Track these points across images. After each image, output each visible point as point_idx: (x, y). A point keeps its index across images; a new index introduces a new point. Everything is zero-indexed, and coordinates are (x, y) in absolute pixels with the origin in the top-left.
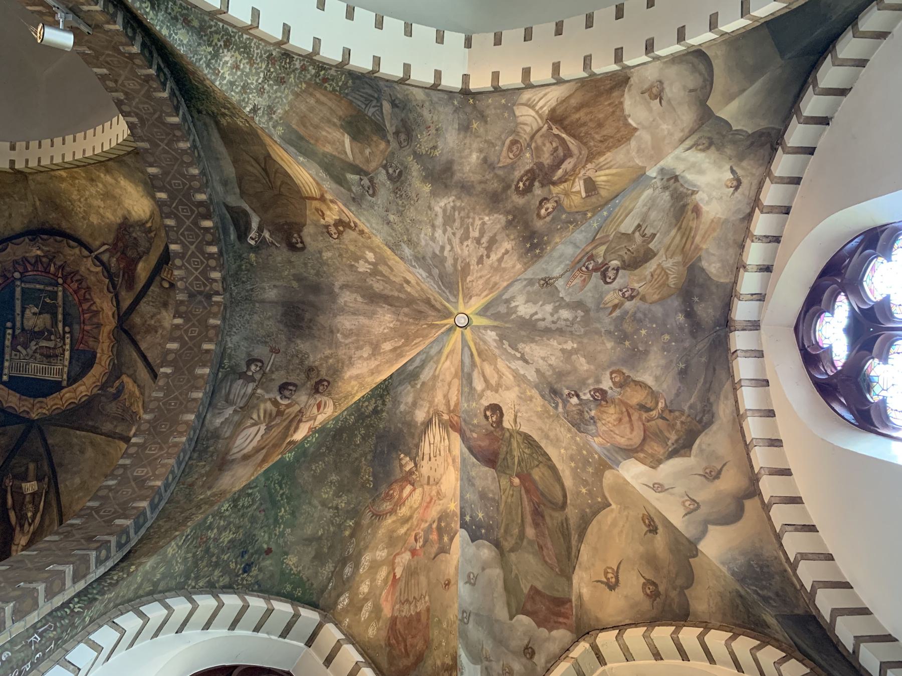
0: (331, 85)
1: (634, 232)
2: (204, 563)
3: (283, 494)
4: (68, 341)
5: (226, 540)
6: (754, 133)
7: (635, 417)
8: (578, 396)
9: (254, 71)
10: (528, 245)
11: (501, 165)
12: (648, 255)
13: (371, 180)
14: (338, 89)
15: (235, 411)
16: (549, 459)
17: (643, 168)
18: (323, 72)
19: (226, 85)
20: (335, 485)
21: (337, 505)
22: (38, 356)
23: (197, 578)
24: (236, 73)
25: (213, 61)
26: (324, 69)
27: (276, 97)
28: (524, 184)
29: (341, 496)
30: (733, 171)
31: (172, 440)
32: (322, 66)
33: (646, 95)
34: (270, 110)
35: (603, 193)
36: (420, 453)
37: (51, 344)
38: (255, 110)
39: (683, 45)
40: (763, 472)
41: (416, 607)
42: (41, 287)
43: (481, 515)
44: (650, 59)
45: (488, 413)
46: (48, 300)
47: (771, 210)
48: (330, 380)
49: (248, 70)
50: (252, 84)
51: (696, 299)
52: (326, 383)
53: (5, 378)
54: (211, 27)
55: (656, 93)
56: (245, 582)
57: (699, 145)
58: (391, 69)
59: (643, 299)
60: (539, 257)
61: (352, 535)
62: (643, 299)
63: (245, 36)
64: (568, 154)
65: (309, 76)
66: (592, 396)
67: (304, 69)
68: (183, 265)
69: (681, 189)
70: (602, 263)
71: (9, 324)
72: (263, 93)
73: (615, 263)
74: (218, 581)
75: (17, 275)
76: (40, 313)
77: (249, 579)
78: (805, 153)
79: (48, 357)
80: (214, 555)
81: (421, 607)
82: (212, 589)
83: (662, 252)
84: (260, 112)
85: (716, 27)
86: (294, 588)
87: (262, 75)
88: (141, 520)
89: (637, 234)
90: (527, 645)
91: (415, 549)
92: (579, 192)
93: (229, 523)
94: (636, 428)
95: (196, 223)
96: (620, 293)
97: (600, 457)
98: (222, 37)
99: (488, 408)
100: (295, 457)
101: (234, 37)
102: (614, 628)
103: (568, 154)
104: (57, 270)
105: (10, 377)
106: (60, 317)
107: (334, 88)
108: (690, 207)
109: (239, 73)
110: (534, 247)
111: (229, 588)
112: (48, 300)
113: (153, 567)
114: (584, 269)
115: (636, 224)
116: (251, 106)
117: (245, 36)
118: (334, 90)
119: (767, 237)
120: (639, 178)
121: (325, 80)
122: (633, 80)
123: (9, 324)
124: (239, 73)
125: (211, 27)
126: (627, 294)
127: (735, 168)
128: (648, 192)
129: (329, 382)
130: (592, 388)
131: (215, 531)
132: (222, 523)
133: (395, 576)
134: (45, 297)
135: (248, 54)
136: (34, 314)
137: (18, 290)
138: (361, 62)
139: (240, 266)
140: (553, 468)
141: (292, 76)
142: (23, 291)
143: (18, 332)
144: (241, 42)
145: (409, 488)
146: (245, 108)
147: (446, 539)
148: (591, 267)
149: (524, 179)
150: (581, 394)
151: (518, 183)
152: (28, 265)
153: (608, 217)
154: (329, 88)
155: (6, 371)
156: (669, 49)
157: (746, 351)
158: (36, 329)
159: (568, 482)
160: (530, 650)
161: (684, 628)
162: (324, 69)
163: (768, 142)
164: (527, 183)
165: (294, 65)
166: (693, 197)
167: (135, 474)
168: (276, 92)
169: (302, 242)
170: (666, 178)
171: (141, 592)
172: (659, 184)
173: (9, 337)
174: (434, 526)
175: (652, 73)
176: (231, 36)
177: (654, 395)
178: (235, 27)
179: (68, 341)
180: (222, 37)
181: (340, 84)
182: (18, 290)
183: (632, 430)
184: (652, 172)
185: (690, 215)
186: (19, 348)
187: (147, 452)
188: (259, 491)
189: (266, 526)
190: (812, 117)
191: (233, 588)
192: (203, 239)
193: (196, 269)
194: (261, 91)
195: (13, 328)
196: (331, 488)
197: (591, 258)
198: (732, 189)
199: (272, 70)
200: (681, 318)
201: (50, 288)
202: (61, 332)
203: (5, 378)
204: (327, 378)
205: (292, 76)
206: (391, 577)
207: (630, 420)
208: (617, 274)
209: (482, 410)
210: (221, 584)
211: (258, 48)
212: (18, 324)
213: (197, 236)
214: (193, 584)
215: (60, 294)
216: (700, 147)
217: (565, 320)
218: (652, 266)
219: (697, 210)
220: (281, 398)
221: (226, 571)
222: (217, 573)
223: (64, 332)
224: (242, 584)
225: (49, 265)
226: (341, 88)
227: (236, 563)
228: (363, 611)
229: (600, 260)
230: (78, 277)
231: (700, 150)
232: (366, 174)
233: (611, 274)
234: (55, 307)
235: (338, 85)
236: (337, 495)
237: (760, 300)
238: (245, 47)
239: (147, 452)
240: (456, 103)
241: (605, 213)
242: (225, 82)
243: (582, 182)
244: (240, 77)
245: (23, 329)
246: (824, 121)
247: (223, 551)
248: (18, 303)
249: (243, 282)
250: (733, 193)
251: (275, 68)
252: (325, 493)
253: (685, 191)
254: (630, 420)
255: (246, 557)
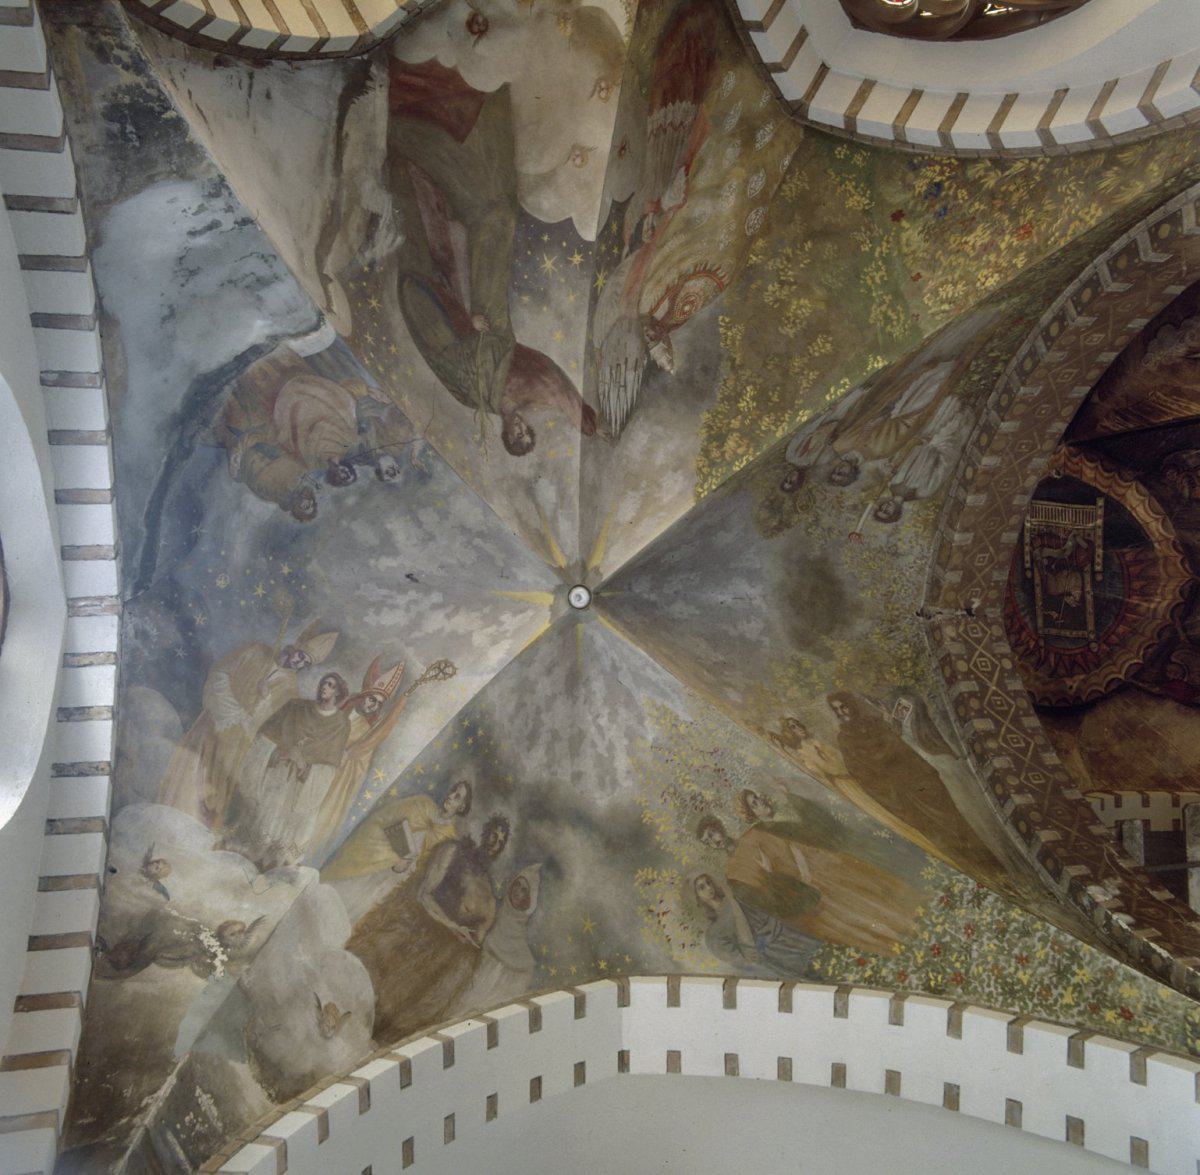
0: (849, 957)
1: (309, 766)
2: (1015, 198)
3: (880, 305)
4: (1027, 558)
5: (979, 231)
6: (147, 965)
7: (285, 435)
8: (378, 472)
9: (990, 958)
10: (480, 732)
11: (537, 866)
12: (271, 727)
13: (751, 816)
14: (836, 953)
15: (929, 440)
16: (428, 360)
17: (323, 880)
18: (869, 973)
19: (1037, 930)
20: (788, 318)
21: (782, 288)
22: (1062, 535)
23: (1027, 174)
24: (1022, 949)
25: (1065, 962)
26: (866, 980)
27: (942, 924)
28: (496, 836)
29: (775, 302)
30: (163, 891)
31: (1037, 391)
32: (874, 982)
33: (342, 1011)
34: (950, 901)
35: (378, 832)
36: (640, 371)
37: (1048, 552)
38: (978, 899)
39: (315, 1108)
40: (91, 321)
41: (665, 117)
42: (1063, 633)
43: (548, 264)
44: (355, 1074)
45: (527, 439)
46: (1055, 615)
47: (83, 826)
48: (778, 491)
49: (1001, 958)
50: (989, 939)
51: (180, 653)
52: (787, 486)
53: (1101, 502)
54: (1080, 1013)
55: (329, 1019)
56: (937, 168)
57: (241, 931)
58: (757, 995)
59: (268, 651)
60: (463, 714)
61: (752, 239)
62: (268, 651)
63: (1017, 1009)
64: (439, 894)
65: (890, 965)
66: (353, 472)
67: (902, 976)
68: (1000, 660)
69: (245, 850)
70: (350, 711)
71: (1099, 578)
72: (968, 927)
73: (328, 712)
74: (987, 170)
75: (1094, 645)
76: (1062, 595)
77: (929, 174)
78: (45, 938)
79: (1051, 535)
80: (1000, 209)
81: (658, 116)
82: (1000, 158)
83: (251, 735)
84: (967, 896)
85: (279, 1150)
86: (848, 158)
87: (975, 955)
88: (1122, 263)
89: (301, 765)
90: (479, 37)
91: (655, 212)
92: (414, 830)
93: (977, 258)
94: (287, 414)
95: (998, 724)
96: (307, 659)
97: (362, 361)
98: (1056, 1001)
99: (529, 448)
100: (866, 364)
101: (1035, 1005)
102: (326, 56)
103: (439, 894)
104: (1046, 659)
105: (1095, 504)
106: (1038, 590)
107: (844, 953)
108: (220, 819)
109: (1016, 951)
110: (470, 731)
111: (967, 159)
112: (1055, 615)
113: (1127, 185)
114: (379, 698)
115: (308, 783)
116: (985, 903)
117: (1017, 1009)
118: (842, 949)
119: (82, 774)
120: (333, 863)
121: (861, 963)
122: (366, 1034)
123: (1099, 578)
124: (1016, 951)
125: (1080, 1013)
126: (296, 658)
127: (161, 897)
128: (305, 839)
129: (782, 488)
130: (351, 487)
131: (1003, 246)
132: (992, 257)
133: (687, 170)
134: (1057, 619)
135: (1006, 983)
136: (1069, 594)
137: (1091, 627)
138: (813, 999)
139: (915, 665)
140: (424, 347)
141: (920, 961)
142: (1083, 625)
143: (1087, 568)
144: (1022, 999)
145: (659, 314)
146: (996, 900)
147: (614, 227)
148: (368, 702)
149: (496, 847)
150: (372, 475)
151: (506, 838)
152: (1081, 661)
153: (362, 790)
154: (851, 952)
155: (1100, 512)
156: (333, 1096)
157: (96, 557)
158: (1065, 573)
159: (397, 319)
160: (476, 28)
161: (225, 39)
162: (866, 980)
163: (126, 949)
164: (492, 839)
165: (920, 979)
166: (220, 838)
167: (1103, 336)
168: (945, 932)
169: (835, 709)
170: (280, 867)
171: (1140, 149)
172: (288, 855)
173: (1099, 560)
174: (626, 249)
175: (340, 1050)
176: (1041, 1005)
177: (248, 477)
178: (1040, 1020)
179: (1027, 558)
180: (1056, 1001)
181: (833, 961)
182: (1091, 627)
183: (294, 410)
184: (308, 875)
185: (219, 806)
186: (1084, 545)
187: (1075, 371)
188: (928, 307)
189: (906, 255)
190: (59, 1006)
191: (957, 159)
192: (981, 699)
193: (981, 655)
194: (971, 929)
195: (1094, 573)
196: (796, 316)
197: (371, 718)
198: (155, 857)
199: (958, 965)
200: (200, 620)
201: (1054, 631)
202: (1036, 570)
203: (1101, 502)
204: (785, 495)
205: (920, 961)
206: (692, 169)
207: (294, 428)
208: (320, 691)
209: (537, 445)
210: (981, 166)
211: (990, 994)
212: (1088, 578)
213: (990, 704)
214: (1034, 165)
215: (1040, 622)
216: (237, 928)
217: (396, 607)
218: (265, 707)
219: (208, 815)
220: (857, 460)
221: (974, 187)
222: (991, 183)
223: (1032, 570)
224: (942, 165)
225: (1057, 664)
226: (830, 955)
227: (955, 197)
228: (737, 117)
229: (354, 715)
230: (1021, 649)
231: (235, 923)
232: (761, 827)
233: (329, 692)
234: (1045, 607)
235: (838, 957)
236: (784, 304)
237: (74, 655)
238: (1012, 993)
239: (1075, 371)
240: (628, 960)
241: (368, 795)
242: (1039, 934)
243: (411, 847)
244: (1012, 946)
245: (1081, 571)
246: (27, 1003)
247: (984, 215)
248: (1090, 608)
249: (906, 641)
250: (151, 850)
251: (953, 968)
252: (805, 307)
253: (238, 848)
254: (294, 428)
255: (938, 207)
